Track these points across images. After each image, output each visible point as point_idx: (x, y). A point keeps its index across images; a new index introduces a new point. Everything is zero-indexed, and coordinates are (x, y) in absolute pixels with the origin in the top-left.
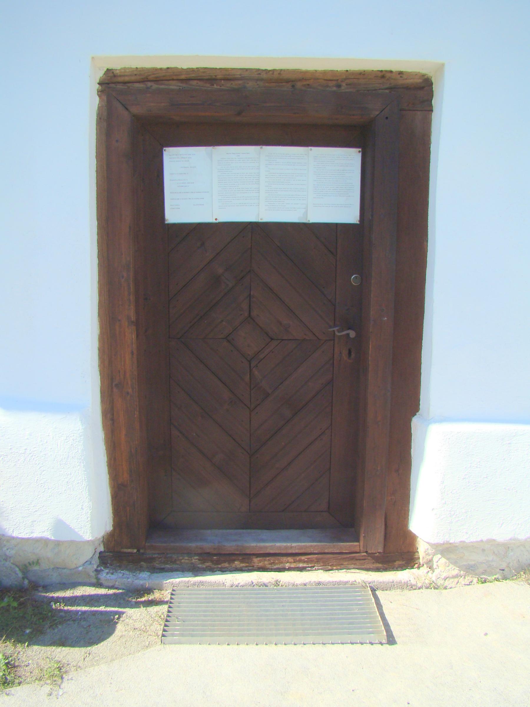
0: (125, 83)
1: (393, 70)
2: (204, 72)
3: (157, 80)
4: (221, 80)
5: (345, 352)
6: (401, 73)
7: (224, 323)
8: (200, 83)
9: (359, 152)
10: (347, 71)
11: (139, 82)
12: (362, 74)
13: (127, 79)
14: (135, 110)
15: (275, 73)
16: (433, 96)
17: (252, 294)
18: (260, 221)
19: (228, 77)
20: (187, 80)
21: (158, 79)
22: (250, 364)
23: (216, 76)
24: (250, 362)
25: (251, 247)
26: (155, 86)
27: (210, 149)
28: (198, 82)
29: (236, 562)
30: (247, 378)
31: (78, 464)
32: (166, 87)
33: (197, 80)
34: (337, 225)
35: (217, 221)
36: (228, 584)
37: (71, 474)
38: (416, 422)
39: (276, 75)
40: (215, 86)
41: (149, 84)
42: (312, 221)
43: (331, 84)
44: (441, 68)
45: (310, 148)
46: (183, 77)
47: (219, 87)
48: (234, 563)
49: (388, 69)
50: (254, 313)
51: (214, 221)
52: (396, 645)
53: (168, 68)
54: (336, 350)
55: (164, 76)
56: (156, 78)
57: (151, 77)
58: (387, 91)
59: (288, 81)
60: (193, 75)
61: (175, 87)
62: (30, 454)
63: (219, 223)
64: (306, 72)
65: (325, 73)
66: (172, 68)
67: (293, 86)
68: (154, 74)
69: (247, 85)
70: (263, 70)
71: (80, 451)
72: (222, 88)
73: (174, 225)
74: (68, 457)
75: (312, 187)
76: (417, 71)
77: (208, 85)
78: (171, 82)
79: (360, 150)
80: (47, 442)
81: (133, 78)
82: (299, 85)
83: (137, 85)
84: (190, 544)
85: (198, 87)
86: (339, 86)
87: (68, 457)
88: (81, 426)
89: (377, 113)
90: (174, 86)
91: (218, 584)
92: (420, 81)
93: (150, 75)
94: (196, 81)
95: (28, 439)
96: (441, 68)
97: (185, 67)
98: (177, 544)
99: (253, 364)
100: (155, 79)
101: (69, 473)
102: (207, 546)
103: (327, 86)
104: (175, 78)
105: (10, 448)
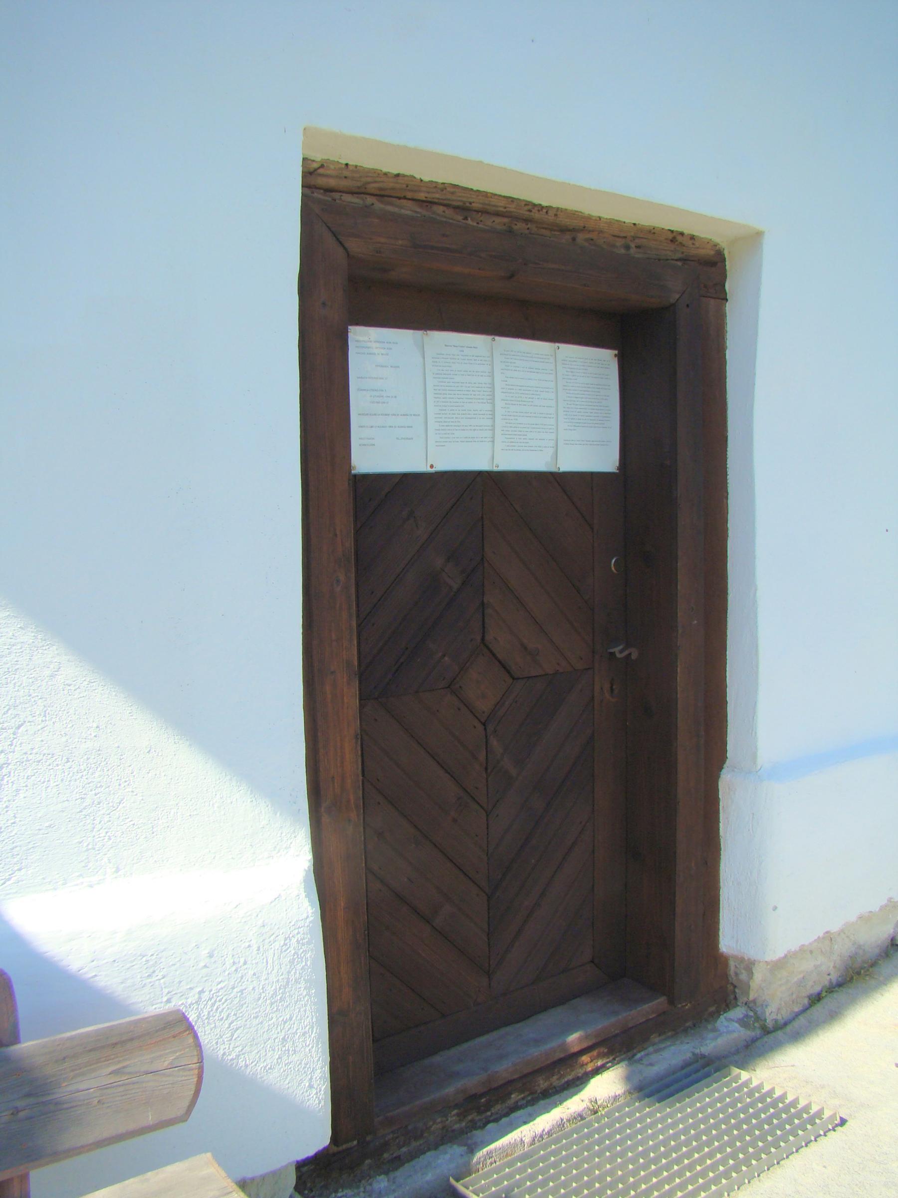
0: (328, 190)
1: (686, 232)
2: (453, 193)
3: (381, 195)
4: (477, 211)
5: (607, 686)
6: (692, 238)
7: (446, 658)
8: (449, 212)
9: (616, 355)
10: (634, 224)
11: (352, 193)
12: (652, 232)
13: (332, 183)
14: (355, 246)
15: (551, 213)
16: (726, 277)
17: (485, 601)
18: (495, 469)
19: (488, 207)
20: (428, 203)
21: (382, 193)
22: (485, 729)
23: (470, 203)
24: (484, 724)
25: (482, 518)
26: (378, 205)
27: (419, 333)
28: (445, 208)
29: (513, 1096)
30: (482, 757)
31: (305, 993)
32: (396, 210)
33: (445, 205)
34: (592, 475)
35: (433, 470)
36: (527, 1140)
37: (291, 1019)
38: (727, 779)
39: (550, 218)
40: (469, 222)
41: (370, 200)
42: (562, 469)
43: (619, 243)
44: (754, 238)
45: (557, 344)
46: (422, 196)
47: (475, 224)
48: (510, 1098)
49: (680, 230)
50: (489, 637)
51: (429, 470)
52: (848, 1123)
53: (398, 175)
54: (597, 688)
55: (393, 189)
56: (381, 189)
57: (372, 188)
58: (680, 264)
59: (564, 230)
60: (437, 196)
61: (408, 213)
62: (210, 999)
63: (437, 473)
64: (589, 218)
65: (610, 222)
66: (404, 176)
67: (574, 239)
68: (375, 182)
69: (515, 227)
70: (534, 205)
71: (309, 963)
72: (480, 226)
73: (365, 477)
74: (288, 983)
75: (523, 409)
76: (709, 237)
77: (460, 218)
78: (404, 202)
79: (616, 352)
80: (245, 963)
81: (343, 184)
82: (581, 237)
83: (348, 198)
84: (447, 1091)
85: (445, 220)
86: (628, 247)
87: (288, 983)
88: (310, 908)
89: (677, 296)
90: (408, 209)
91: (513, 1146)
92: (712, 253)
93: (369, 183)
94: (441, 208)
95: (205, 966)
96: (754, 238)
97: (426, 179)
98: (427, 1099)
99: (490, 728)
100: (378, 193)
101: (288, 1016)
102: (471, 1082)
103: (614, 246)
104: (409, 195)
105: (165, 999)
